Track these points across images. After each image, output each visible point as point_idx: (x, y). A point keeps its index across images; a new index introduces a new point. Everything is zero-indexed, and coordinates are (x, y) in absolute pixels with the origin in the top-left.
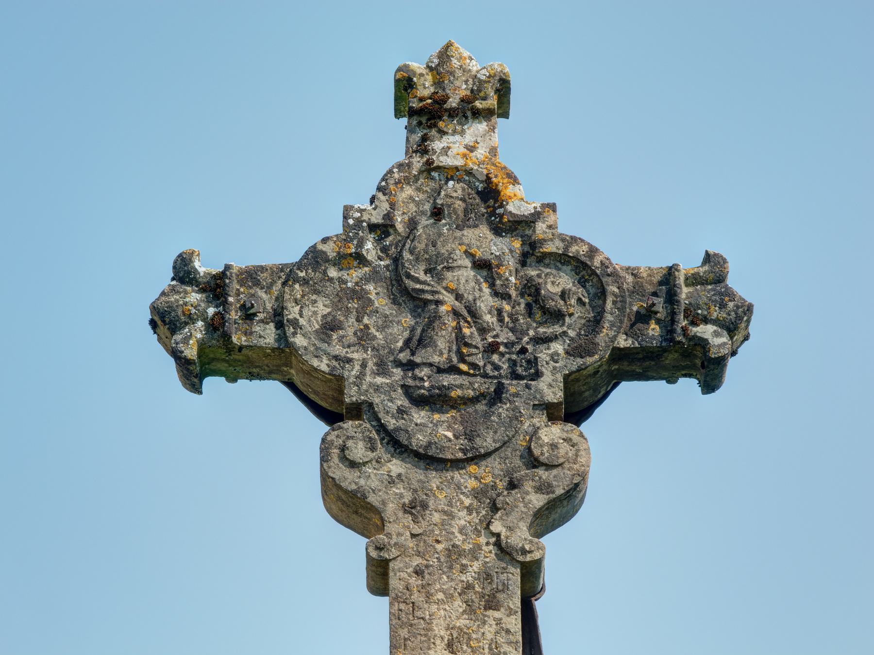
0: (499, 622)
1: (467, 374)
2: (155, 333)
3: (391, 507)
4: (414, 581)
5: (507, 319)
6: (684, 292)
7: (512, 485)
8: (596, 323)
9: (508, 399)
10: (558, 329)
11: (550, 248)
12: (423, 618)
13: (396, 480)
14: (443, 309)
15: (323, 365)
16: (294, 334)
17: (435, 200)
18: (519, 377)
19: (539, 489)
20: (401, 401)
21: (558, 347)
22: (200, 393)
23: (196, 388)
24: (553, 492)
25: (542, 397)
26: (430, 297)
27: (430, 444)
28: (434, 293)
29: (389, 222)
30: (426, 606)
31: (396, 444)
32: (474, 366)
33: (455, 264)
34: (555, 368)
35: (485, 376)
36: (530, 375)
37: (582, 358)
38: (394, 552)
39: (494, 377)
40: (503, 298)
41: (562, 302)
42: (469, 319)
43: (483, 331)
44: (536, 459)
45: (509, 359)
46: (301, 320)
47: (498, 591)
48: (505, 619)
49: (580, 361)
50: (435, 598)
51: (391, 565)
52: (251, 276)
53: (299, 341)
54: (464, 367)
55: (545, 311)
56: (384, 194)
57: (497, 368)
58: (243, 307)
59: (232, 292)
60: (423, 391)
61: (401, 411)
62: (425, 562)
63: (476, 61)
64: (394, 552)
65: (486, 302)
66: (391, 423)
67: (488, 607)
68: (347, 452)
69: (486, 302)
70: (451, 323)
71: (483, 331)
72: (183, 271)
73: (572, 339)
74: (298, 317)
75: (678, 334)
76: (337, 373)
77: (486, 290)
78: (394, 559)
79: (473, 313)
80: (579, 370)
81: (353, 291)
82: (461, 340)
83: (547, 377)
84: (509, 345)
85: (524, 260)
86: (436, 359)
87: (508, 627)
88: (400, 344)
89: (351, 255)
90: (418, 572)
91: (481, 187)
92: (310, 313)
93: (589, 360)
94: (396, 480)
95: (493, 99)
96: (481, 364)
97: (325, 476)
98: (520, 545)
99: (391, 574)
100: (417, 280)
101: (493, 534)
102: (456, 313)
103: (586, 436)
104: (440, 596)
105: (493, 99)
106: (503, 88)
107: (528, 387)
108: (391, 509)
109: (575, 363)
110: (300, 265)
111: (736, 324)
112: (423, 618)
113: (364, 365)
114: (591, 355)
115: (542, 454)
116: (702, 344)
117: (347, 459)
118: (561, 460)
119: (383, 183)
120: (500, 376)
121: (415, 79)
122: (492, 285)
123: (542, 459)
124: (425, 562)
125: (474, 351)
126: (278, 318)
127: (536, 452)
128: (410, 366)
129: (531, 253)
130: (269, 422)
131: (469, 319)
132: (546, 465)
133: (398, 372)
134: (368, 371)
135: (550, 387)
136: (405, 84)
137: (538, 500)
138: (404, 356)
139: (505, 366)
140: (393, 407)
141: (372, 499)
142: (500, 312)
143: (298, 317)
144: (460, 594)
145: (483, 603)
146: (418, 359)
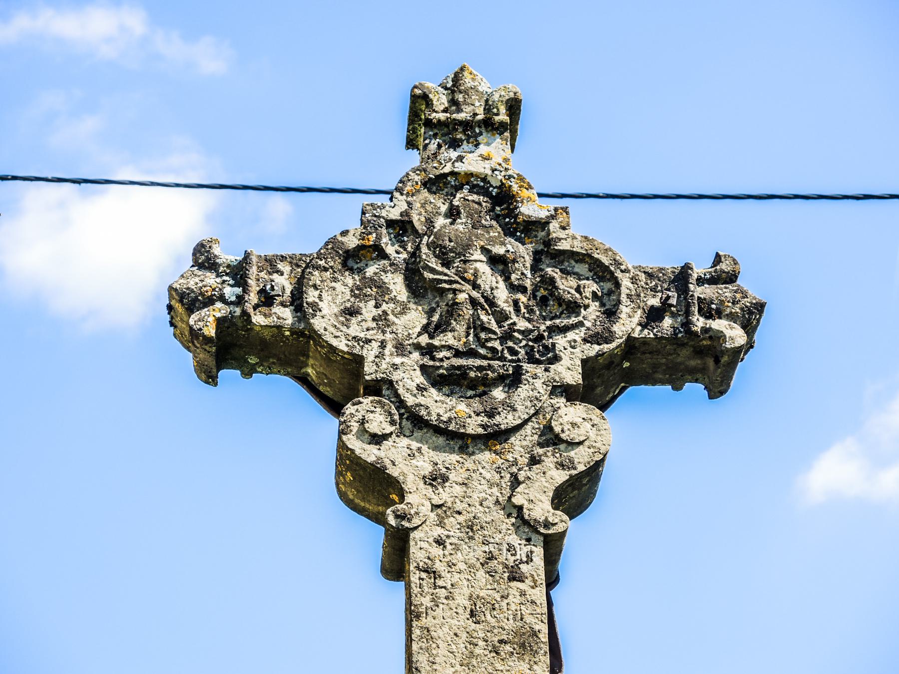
0: (523, 594)
1: (484, 357)
2: (169, 313)
3: (410, 478)
4: (437, 551)
5: (523, 310)
6: (699, 291)
7: (534, 461)
8: (611, 314)
9: (527, 380)
10: (573, 320)
11: (564, 246)
12: (445, 587)
13: (417, 454)
14: (462, 297)
15: (342, 345)
16: (314, 316)
17: (452, 201)
18: (538, 362)
19: (561, 465)
20: (419, 379)
21: (575, 335)
22: (216, 385)
23: (210, 378)
24: (575, 469)
25: (560, 379)
26: (447, 286)
27: (450, 420)
28: (451, 282)
29: (406, 218)
30: (449, 575)
31: (415, 421)
32: (493, 350)
33: (472, 258)
34: (572, 353)
35: (502, 358)
36: (548, 359)
37: (599, 344)
38: (416, 522)
39: (511, 361)
40: (518, 291)
41: (578, 296)
42: (486, 306)
43: (501, 317)
44: (557, 436)
45: (527, 345)
46: (320, 303)
47: (521, 562)
48: (530, 591)
49: (597, 348)
50: (457, 567)
51: (412, 535)
52: (271, 264)
53: (318, 323)
54: (482, 351)
55: (560, 301)
56: (402, 194)
57: (513, 352)
58: (262, 292)
59: (253, 277)
60: (441, 371)
61: (420, 389)
62: (446, 533)
63: (487, 84)
64: (416, 522)
65: (502, 295)
66: (410, 401)
67: (512, 579)
68: (366, 425)
69: (502, 295)
70: (468, 312)
71: (501, 317)
72: (203, 258)
73: (588, 329)
74: (317, 300)
75: (687, 347)
76: (357, 351)
77: (502, 285)
78: (416, 528)
79: (491, 303)
80: (598, 355)
81: (371, 279)
82: (477, 327)
83: (566, 361)
84: (525, 333)
85: (537, 257)
86: (451, 342)
87: (534, 598)
88: (418, 329)
89: (370, 246)
90: (440, 542)
91: (495, 192)
92: (329, 299)
93: (606, 347)
94: (417, 454)
95: (505, 120)
96: (500, 348)
97: (342, 446)
98: (543, 518)
99: (412, 543)
100: (433, 271)
101: (515, 506)
102: (473, 302)
103: (564, 566)
104: (462, 566)
105: (505, 120)
106: (514, 106)
107: (546, 370)
108: (411, 482)
109: (593, 350)
110: (319, 256)
111: (751, 317)
112: (445, 587)
113: (383, 345)
114: (608, 341)
115: (563, 431)
116: (717, 337)
117: (367, 432)
118: (582, 439)
119: (400, 185)
120: (519, 360)
121: (430, 96)
122: (507, 279)
123: (563, 436)
124: (446, 533)
125: (493, 336)
126: (297, 300)
127: (557, 429)
128: (429, 351)
129: (547, 253)
130: (282, 433)
131: (486, 306)
132: (566, 442)
133: (416, 355)
134: (387, 352)
135: (569, 371)
136: (420, 101)
137: (561, 477)
138: (424, 340)
139: (523, 352)
140: (412, 386)
141: (393, 472)
142: (516, 303)
143: (317, 300)
144: (482, 565)
145: (506, 575)
146: (436, 342)
